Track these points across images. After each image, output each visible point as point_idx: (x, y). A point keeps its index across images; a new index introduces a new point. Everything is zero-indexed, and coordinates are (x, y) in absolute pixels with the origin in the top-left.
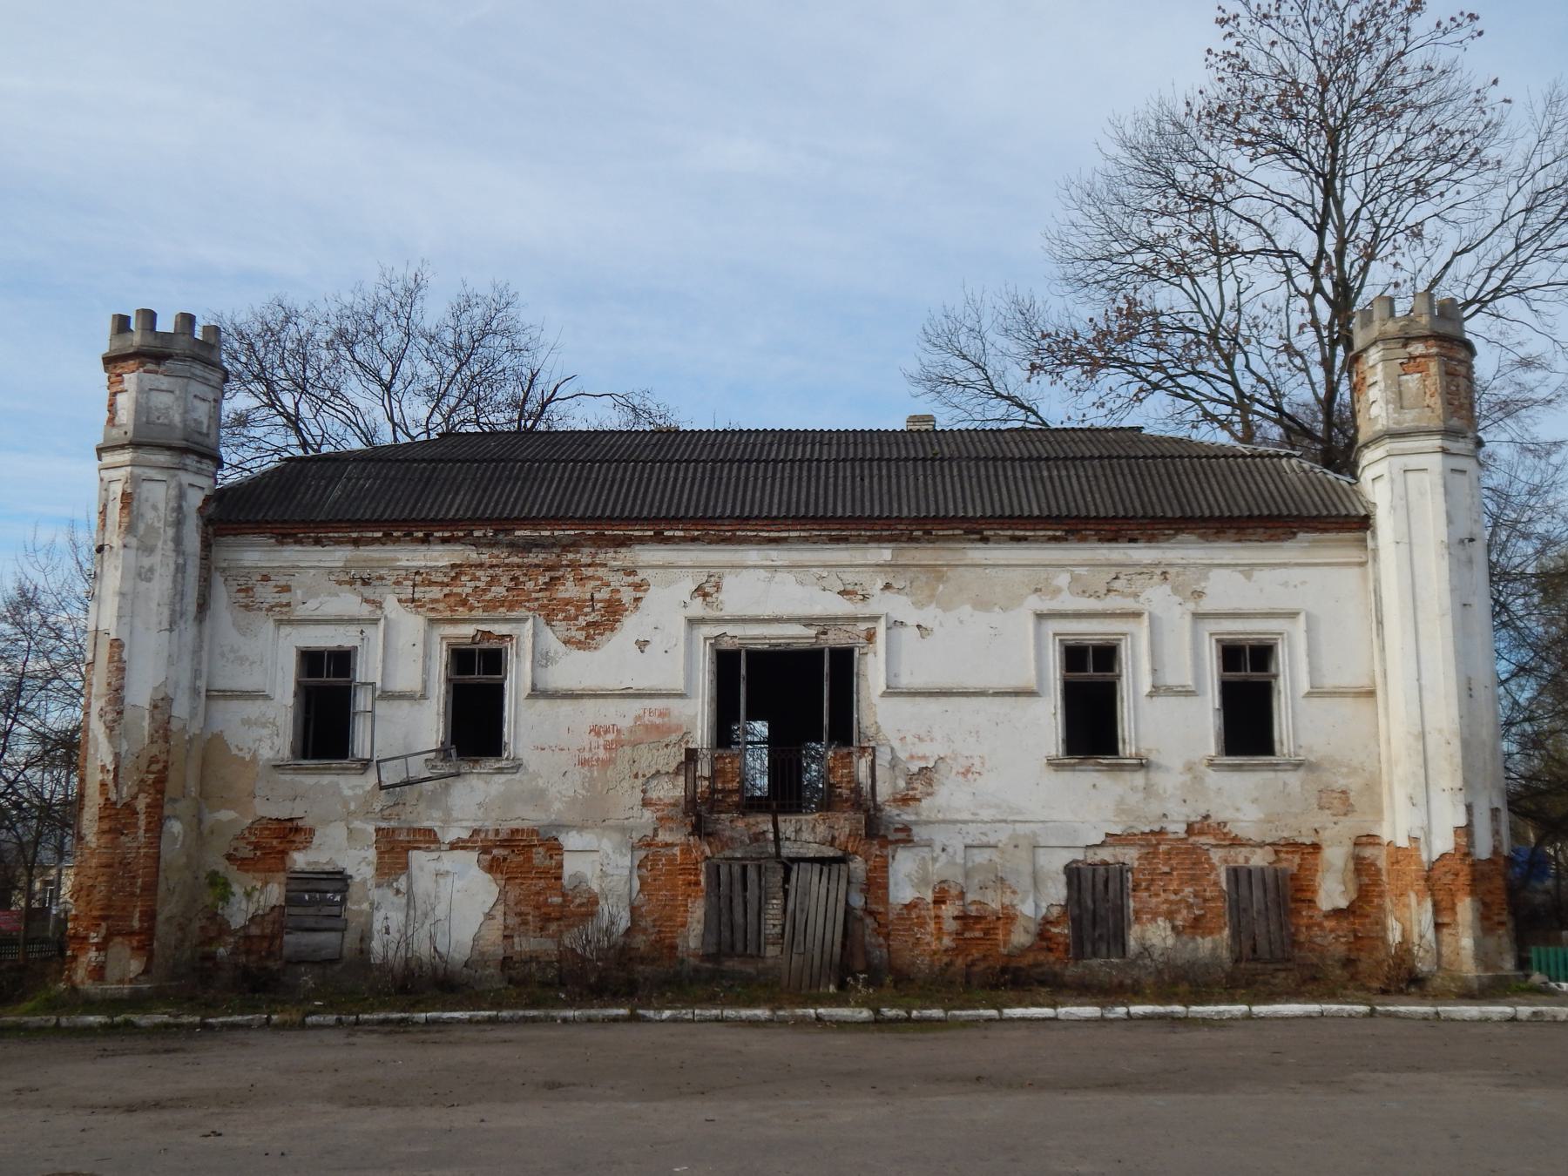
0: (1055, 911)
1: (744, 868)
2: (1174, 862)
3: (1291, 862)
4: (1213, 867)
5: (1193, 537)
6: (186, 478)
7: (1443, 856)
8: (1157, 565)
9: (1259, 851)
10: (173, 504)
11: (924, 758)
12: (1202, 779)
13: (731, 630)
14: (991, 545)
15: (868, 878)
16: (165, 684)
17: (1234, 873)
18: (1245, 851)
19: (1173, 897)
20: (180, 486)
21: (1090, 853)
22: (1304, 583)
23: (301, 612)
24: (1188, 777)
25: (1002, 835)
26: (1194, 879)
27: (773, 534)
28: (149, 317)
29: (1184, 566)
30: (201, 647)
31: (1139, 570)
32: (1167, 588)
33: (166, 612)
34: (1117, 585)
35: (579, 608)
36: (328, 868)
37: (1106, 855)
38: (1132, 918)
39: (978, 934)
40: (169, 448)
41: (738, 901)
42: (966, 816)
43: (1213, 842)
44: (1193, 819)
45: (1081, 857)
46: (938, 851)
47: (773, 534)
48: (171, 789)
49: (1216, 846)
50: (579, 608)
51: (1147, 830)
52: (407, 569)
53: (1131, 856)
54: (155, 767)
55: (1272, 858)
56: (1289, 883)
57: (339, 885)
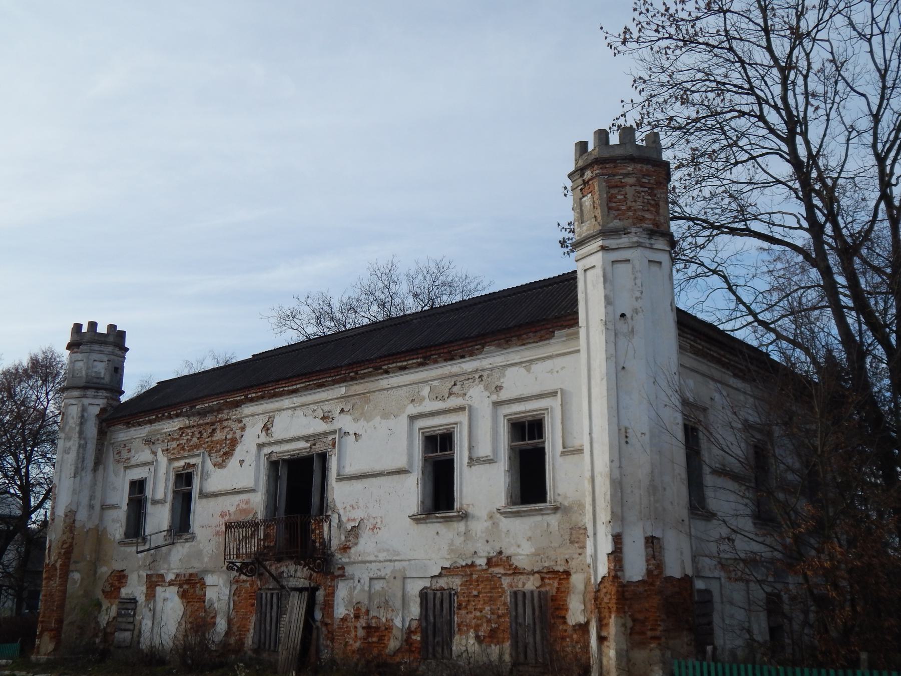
0: (415, 624)
1: (272, 595)
2: (480, 587)
3: (552, 586)
4: (504, 591)
5: (493, 348)
6: (86, 401)
7: (603, 578)
8: (476, 371)
9: (532, 578)
10: (79, 415)
11: (354, 520)
12: (498, 524)
13: (276, 449)
14: (391, 375)
15: (325, 601)
16: (70, 504)
17: (515, 594)
18: (523, 578)
19: (478, 614)
20: (83, 405)
21: (434, 581)
22: (563, 368)
23: (133, 461)
24: (489, 523)
25: (387, 571)
26: (492, 600)
27: (290, 388)
28: (93, 325)
29: (491, 369)
30: (95, 484)
31: (467, 377)
32: (481, 386)
33: (73, 468)
34: (455, 389)
35: (221, 445)
36: (131, 597)
37: (442, 583)
38: (456, 629)
39: (375, 639)
40: (79, 388)
41: (268, 615)
42: (372, 558)
43: (502, 571)
44: (491, 555)
45: (428, 585)
46: (356, 582)
47: (290, 388)
48: (74, 556)
49: (505, 574)
50: (221, 445)
51: (464, 564)
52: (165, 433)
53: (456, 582)
54: (65, 546)
55: (538, 583)
56: (550, 604)
57: (133, 606)
